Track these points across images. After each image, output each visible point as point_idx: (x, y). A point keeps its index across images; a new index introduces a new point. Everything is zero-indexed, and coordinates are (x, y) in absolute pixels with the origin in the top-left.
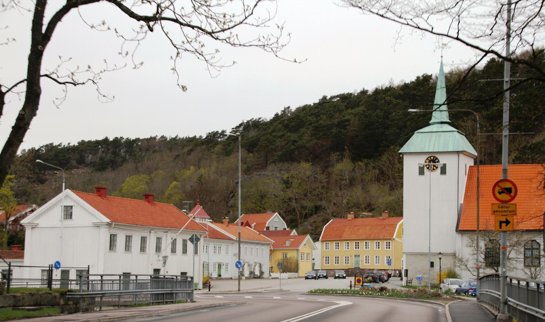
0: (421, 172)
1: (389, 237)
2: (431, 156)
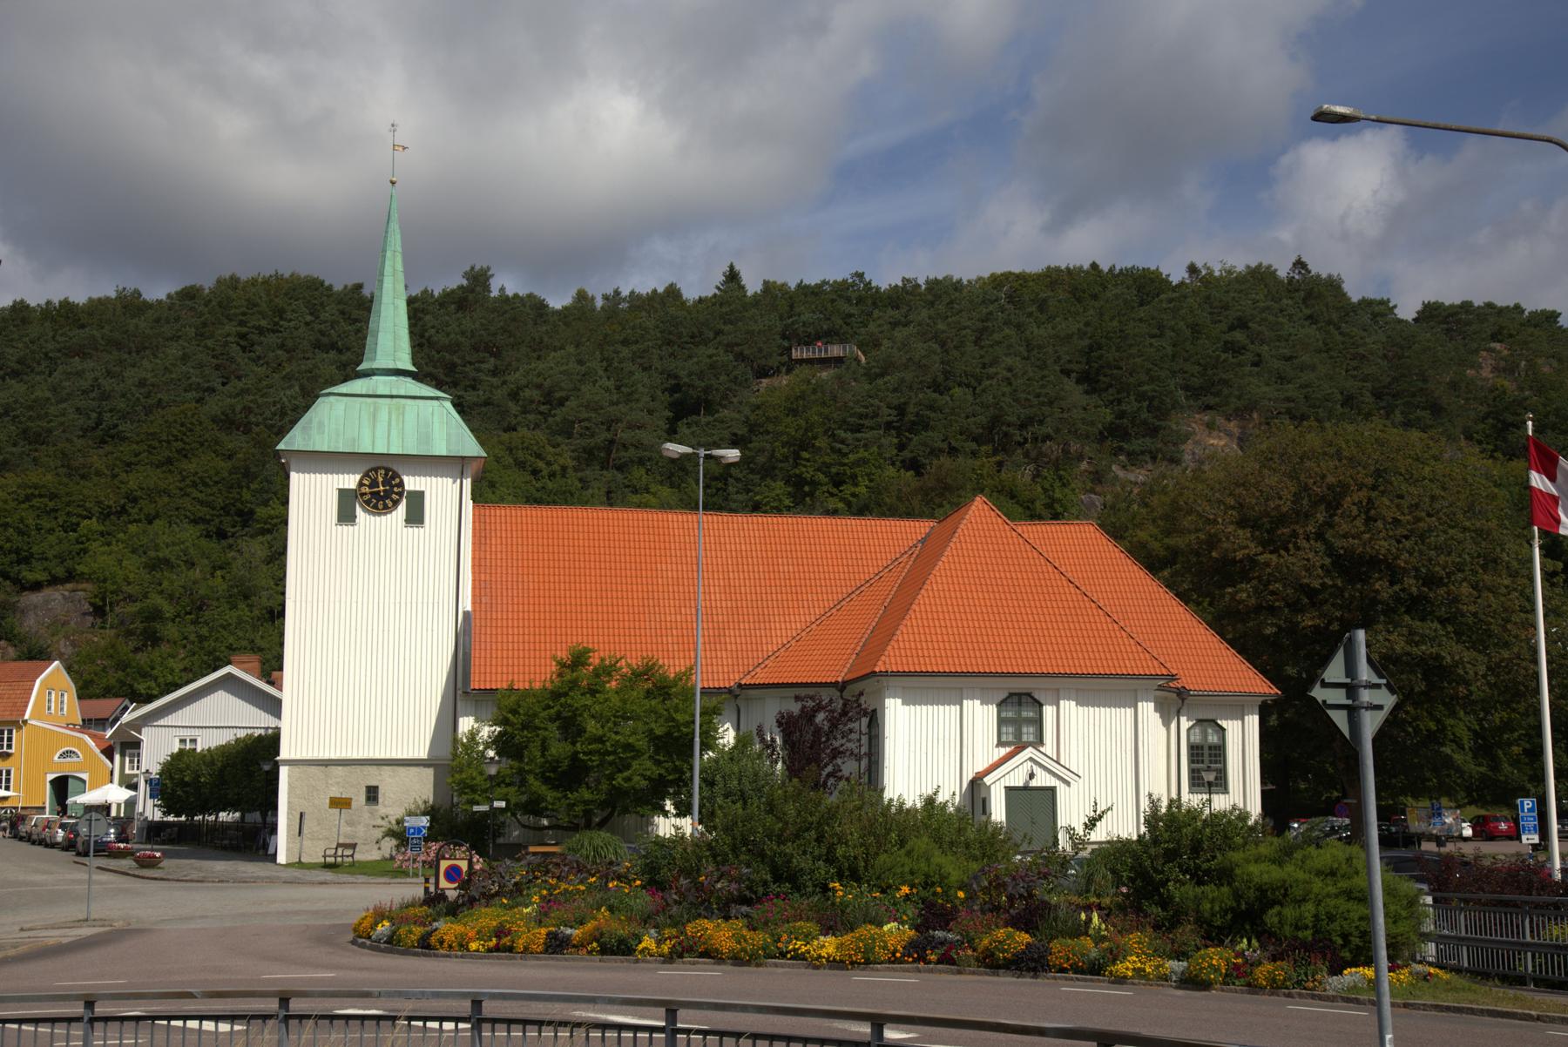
0: (346, 516)
1: (11, 715)
2: (380, 468)
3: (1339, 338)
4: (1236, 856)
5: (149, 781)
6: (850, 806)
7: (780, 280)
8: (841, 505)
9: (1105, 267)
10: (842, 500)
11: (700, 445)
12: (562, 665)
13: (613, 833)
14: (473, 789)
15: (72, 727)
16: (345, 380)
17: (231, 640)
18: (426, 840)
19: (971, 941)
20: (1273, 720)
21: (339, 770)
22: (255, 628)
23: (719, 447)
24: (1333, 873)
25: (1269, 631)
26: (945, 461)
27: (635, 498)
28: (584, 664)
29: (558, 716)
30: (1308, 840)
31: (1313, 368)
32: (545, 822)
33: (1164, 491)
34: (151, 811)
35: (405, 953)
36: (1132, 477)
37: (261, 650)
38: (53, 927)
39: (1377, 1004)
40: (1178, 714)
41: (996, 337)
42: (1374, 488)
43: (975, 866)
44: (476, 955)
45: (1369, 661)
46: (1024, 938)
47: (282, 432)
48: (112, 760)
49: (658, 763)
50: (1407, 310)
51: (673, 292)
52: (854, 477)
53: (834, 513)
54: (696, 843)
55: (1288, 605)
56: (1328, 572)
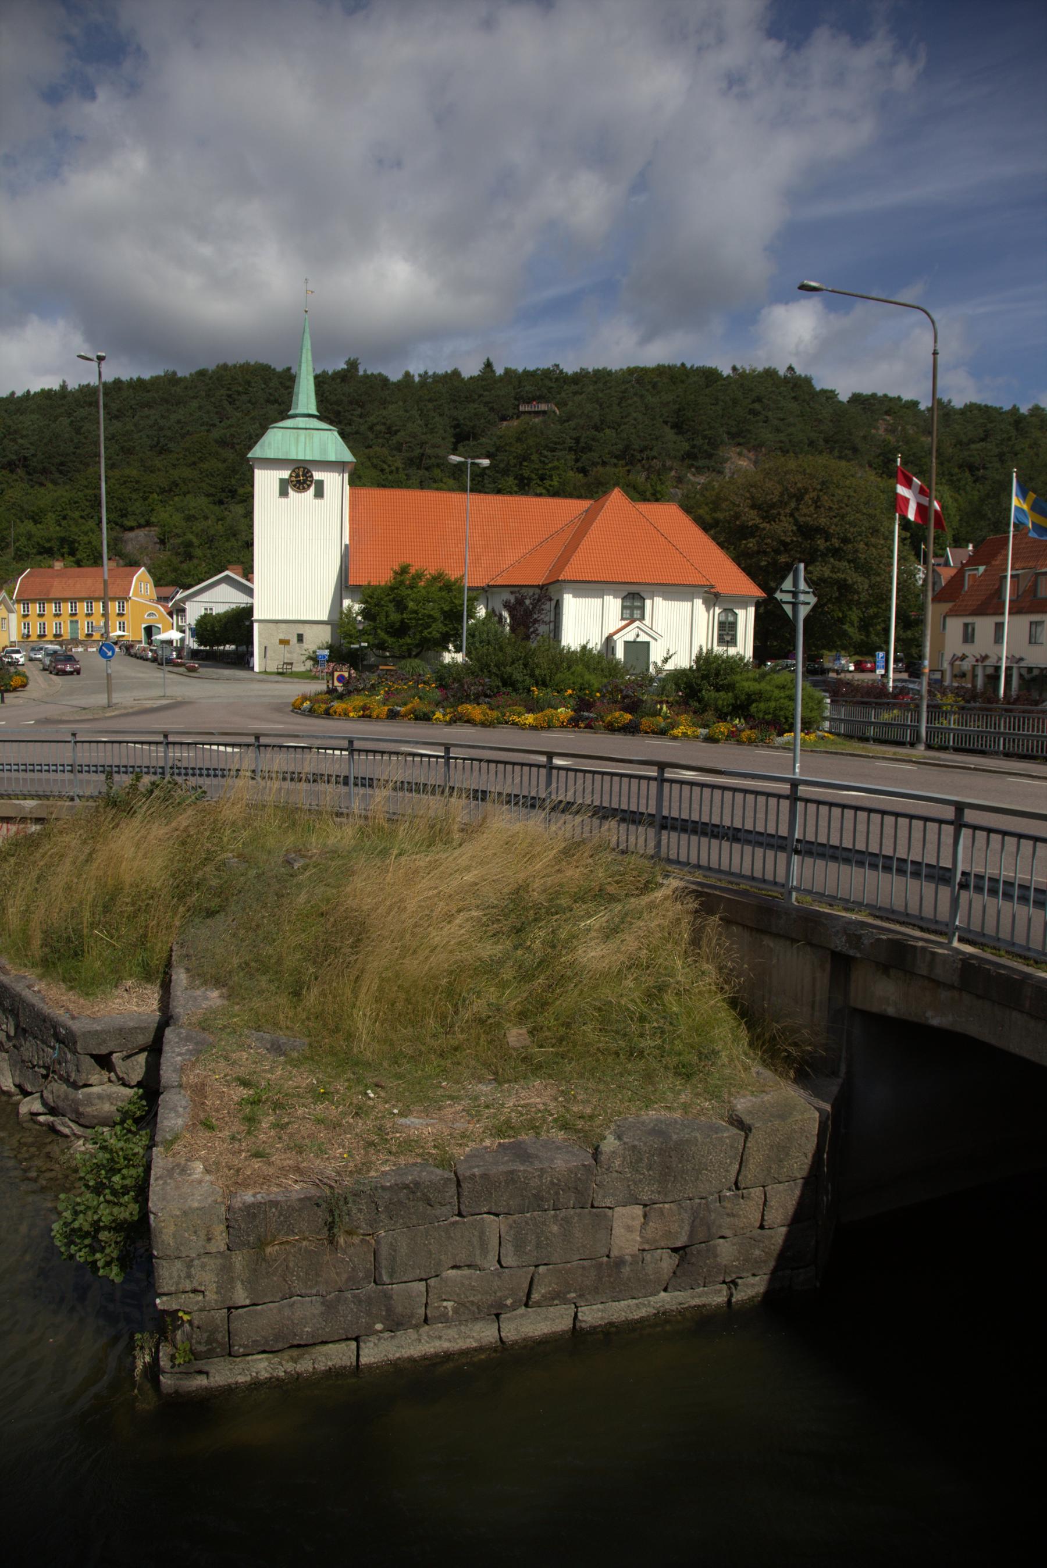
0: (283, 493)
3: (809, 410)
4: (738, 678)
5: (190, 629)
6: (543, 649)
7: (513, 367)
8: (544, 491)
9: (689, 366)
10: (545, 488)
11: (469, 457)
12: (396, 573)
13: (422, 660)
14: (351, 636)
15: (151, 600)
16: (283, 419)
17: (229, 557)
18: (328, 661)
19: (602, 717)
20: (762, 610)
21: (283, 625)
22: (239, 551)
23: (480, 458)
24: (784, 687)
25: (763, 563)
26: (600, 468)
27: (435, 485)
28: (407, 573)
29: (394, 600)
30: (773, 670)
31: (794, 425)
32: (388, 654)
33: (713, 489)
34: (192, 644)
35: (318, 717)
36: (697, 480)
37: (243, 563)
38: (149, 699)
39: (794, 751)
40: (714, 605)
41: (630, 402)
42: (821, 490)
43: (605, 680)
44: (352, 719)
45: (805, 579)
46: (628, 717)
47: (250, 448)
48: (172, 617)
49: (446, 625)
50: (844, 397)
51: (456, 373)
52: (551, 476)
53: (540, 495)
54: (465, 664)
55: (773, 551)
56: (794, 534)
